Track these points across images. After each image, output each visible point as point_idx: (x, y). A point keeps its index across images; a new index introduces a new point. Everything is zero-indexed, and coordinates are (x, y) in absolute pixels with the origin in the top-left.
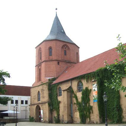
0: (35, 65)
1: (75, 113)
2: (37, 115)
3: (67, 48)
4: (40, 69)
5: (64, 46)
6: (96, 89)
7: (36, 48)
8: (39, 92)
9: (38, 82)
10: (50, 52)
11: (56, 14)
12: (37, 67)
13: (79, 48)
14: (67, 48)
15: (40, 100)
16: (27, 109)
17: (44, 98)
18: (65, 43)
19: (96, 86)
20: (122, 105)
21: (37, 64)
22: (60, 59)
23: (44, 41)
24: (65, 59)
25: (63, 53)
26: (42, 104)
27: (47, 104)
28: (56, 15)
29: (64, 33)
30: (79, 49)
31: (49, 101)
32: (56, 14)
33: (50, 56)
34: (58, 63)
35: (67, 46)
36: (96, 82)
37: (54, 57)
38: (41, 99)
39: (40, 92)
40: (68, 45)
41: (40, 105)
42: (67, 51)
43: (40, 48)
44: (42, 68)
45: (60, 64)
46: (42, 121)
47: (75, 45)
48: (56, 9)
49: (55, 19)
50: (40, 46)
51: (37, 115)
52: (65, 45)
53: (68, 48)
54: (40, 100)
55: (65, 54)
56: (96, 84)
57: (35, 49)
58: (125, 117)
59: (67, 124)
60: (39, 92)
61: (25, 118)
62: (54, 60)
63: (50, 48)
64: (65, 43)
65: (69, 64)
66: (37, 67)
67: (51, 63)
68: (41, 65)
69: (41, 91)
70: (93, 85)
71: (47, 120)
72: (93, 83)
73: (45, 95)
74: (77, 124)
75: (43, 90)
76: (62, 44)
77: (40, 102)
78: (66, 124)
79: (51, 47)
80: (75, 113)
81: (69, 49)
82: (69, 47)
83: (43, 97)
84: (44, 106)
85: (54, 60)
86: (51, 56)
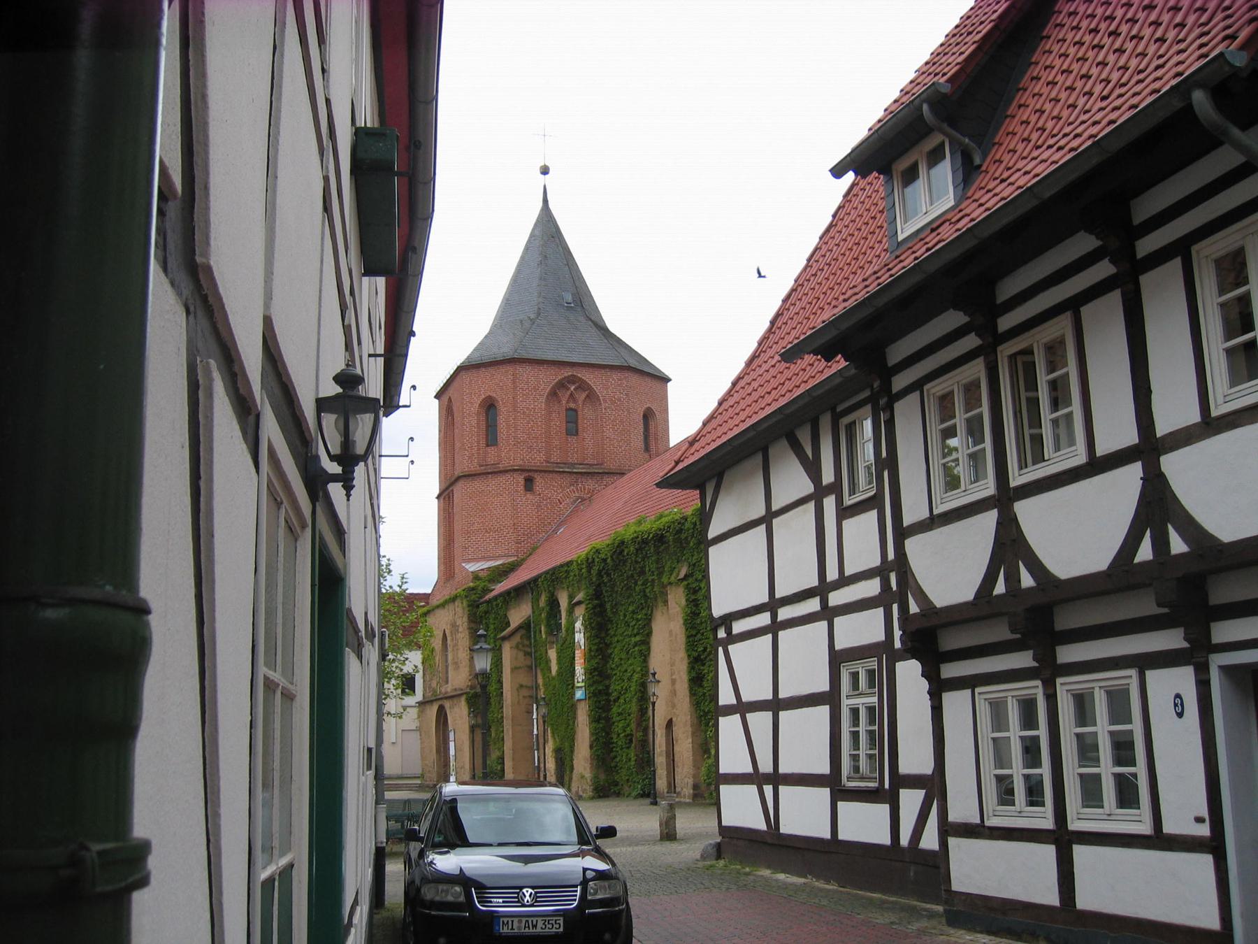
0: (437, 492)
3: (582, 396)
5: (562, 385)
8: (444, 630)
11: (545, 201)
13: (666, 380)
14: (582, 396)
18: (567, 372)
22: (538, 459)
23: (460, 370)
25: (558, 422)
28: (540, 204)
30: (669, 384)
32: (545, 201)
33: (489, 449)
34: (529, 484)
35: (583, 386)
37: (508, 453)
40: (586, 376)
42: (586, 414)
45: (539, 481)
48: (545, 171)
49: (537, 232)
52: (572, 380)
53: (588, 396)
55: (572, 425)
60: (444, 630)
62: (506, 471)
63: (490, 406)
65: (590, 484)
67: (493, 483)
68: (452, 490)
76: (548, 379)
79: (490, 397)
81: (592, 396)
82: (590, 388)
85: (506, 471)
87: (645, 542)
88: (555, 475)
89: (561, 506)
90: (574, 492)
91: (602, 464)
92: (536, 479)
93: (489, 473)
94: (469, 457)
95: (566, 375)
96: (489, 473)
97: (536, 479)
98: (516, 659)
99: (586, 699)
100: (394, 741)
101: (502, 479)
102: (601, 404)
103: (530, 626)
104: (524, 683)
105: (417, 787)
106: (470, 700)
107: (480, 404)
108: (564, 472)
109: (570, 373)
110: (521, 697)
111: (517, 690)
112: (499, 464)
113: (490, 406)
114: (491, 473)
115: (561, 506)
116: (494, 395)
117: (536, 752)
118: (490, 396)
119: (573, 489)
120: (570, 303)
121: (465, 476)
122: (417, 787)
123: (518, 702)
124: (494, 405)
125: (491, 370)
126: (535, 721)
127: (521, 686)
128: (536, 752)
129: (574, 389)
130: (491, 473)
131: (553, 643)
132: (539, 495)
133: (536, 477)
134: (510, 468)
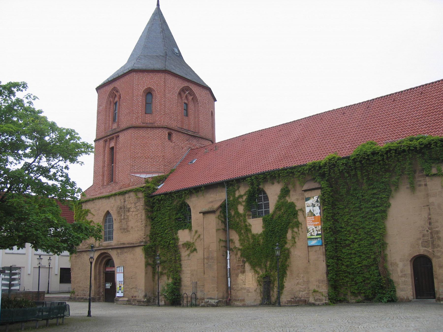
1: (240, 275)
2: (100, 282)
4: (112, 148)
5: (183, 90)
6: (317, 211)
7: (98, 89)
9: (103, 185)
10: (146, 103)
11: (158, 5)
12: (102, 142)
14: (190, 98)
15: (110, 238)
16: (52, 262)
17: (128, 231)
19: (317, 201)
20: (250, 268)
21: (103, 134)
22: (174, 124)
24: (185, 127)
26: (119, 251)
27: (139, 253)
28: (155, 6)
29: (179, 55)
31: (146, 242)
32: (158, 5)
34: (170, 134)
35: (192, 93)
36: (319, 192)
38: (115, 235)
39: (114, 216)
40: (194, 88)
41: (113, 254)
42: (191, 106)
43: (115, 89)
44: (119, 145)
45: (174, 135)
46: (121, 299)
47: (208, 92)
50: (116, 84)
51: (100, 282)
54: (110, 238)
56: (315, 198)
57: (96, 95)
58: (441, 290)
59: (217, 306)
61: (46, 290)
62: (159, 128)
63: (149, 93)
64: (186, 84)
65: (195, 143)
66: (102, 142)
68: (118, 136)
69: (119, 213)
70: (308, 199)
71: (140, 295)
72: (307, 195)
73: (132, 223)
74: (244, 306)
75: (123, 210)
77: (113, 243)
78: (213, 306)
79: (150, 88)
80: (240, 275)
81: (195, 99)
82: (194, 95)
83: (125, 230)
84: (128, 256)
85: (159, 128)
86: (151, 113)
87: (390, 150)
88: (181, 134)
89: (183, 150)
90: (188, 144)
91: (198, 133)
92: (173, 134)
93: (148, 127)
94: (136, 118)
95: (186, 85)
96: (148, 127)
97: (173, 134)
98: (218, 224)
99: (322, 245)
100: (57, 274)
101: (157, 131)
102: (198, 103)
103: (225, 207)
104: (222, 239)
105: (68, 299)
106: (147, 249)
107: (144, 91)
108: (185, 133)
109: (187, 85)
110: (221, 247)
111: (219, 242)
112: (154, 123)
113: (149, 93)
114: (150, 127)
115: (183, 150)
116: (153, 87)
117: (229, 278)
118: (150, 88)
119: (188, 143)
120: (177, 54)
121: (134, 127)
122: (68, 299)
123: (219, 249)
124: (151, 94)
125: (151, 74)
126: (228, 260)
127: (220, 240)
128: (229, 278)
129: (188, 94)
130: (150, 127)
131: (250, 215)
132: (174, 143)
133: (173, 133)
134: (162, 126)
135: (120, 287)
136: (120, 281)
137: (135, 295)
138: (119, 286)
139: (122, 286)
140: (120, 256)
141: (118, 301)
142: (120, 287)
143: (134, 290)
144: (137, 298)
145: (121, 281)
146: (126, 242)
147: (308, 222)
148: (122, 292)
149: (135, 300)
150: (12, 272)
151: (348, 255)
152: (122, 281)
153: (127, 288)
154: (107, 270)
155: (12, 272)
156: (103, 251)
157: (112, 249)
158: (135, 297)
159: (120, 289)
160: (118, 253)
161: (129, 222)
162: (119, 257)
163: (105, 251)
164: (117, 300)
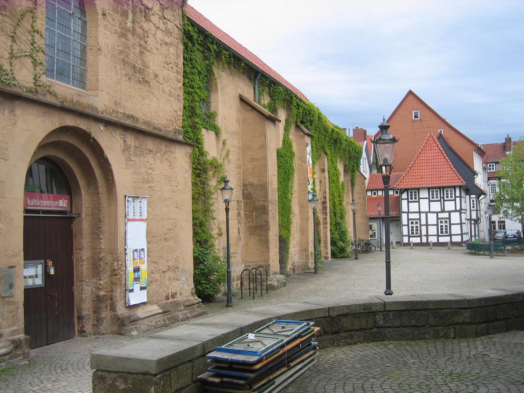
135: (137, 270)
136: (136, 250)
137: (173, 290)
138: (132, 269)
139: (144, 267)
140: (133, 159)
141: (138, 319)
142: (137, 270)
143: (170, 274)
144: (179, 298)
145: (139, 248)
146: (140, 116)
147: (146, 269)
148: (142, 288)
149: (177, 304)
150: (522, 237)
151: (197, 159)
152: (143, 250)
153: (153, 273)
154: (63, 204)
155: (522, 237)
156: (70, 121)
157: (109, 123)
158: (173, 296)
159: (137, 279)
160: (126, 149)
161: (148, 54)
162: (130, 163)
163: (83, 124)
164: (132, 319)
